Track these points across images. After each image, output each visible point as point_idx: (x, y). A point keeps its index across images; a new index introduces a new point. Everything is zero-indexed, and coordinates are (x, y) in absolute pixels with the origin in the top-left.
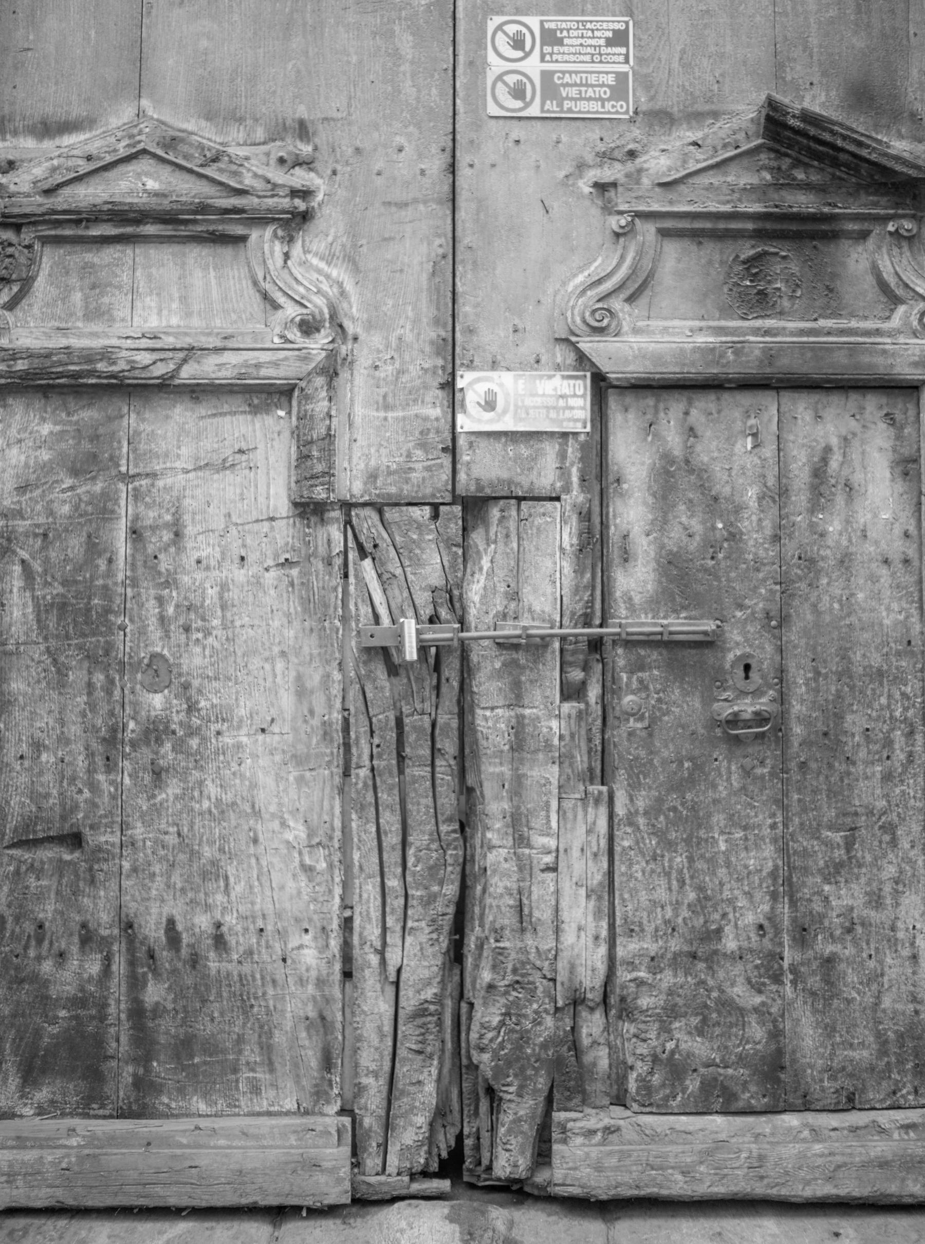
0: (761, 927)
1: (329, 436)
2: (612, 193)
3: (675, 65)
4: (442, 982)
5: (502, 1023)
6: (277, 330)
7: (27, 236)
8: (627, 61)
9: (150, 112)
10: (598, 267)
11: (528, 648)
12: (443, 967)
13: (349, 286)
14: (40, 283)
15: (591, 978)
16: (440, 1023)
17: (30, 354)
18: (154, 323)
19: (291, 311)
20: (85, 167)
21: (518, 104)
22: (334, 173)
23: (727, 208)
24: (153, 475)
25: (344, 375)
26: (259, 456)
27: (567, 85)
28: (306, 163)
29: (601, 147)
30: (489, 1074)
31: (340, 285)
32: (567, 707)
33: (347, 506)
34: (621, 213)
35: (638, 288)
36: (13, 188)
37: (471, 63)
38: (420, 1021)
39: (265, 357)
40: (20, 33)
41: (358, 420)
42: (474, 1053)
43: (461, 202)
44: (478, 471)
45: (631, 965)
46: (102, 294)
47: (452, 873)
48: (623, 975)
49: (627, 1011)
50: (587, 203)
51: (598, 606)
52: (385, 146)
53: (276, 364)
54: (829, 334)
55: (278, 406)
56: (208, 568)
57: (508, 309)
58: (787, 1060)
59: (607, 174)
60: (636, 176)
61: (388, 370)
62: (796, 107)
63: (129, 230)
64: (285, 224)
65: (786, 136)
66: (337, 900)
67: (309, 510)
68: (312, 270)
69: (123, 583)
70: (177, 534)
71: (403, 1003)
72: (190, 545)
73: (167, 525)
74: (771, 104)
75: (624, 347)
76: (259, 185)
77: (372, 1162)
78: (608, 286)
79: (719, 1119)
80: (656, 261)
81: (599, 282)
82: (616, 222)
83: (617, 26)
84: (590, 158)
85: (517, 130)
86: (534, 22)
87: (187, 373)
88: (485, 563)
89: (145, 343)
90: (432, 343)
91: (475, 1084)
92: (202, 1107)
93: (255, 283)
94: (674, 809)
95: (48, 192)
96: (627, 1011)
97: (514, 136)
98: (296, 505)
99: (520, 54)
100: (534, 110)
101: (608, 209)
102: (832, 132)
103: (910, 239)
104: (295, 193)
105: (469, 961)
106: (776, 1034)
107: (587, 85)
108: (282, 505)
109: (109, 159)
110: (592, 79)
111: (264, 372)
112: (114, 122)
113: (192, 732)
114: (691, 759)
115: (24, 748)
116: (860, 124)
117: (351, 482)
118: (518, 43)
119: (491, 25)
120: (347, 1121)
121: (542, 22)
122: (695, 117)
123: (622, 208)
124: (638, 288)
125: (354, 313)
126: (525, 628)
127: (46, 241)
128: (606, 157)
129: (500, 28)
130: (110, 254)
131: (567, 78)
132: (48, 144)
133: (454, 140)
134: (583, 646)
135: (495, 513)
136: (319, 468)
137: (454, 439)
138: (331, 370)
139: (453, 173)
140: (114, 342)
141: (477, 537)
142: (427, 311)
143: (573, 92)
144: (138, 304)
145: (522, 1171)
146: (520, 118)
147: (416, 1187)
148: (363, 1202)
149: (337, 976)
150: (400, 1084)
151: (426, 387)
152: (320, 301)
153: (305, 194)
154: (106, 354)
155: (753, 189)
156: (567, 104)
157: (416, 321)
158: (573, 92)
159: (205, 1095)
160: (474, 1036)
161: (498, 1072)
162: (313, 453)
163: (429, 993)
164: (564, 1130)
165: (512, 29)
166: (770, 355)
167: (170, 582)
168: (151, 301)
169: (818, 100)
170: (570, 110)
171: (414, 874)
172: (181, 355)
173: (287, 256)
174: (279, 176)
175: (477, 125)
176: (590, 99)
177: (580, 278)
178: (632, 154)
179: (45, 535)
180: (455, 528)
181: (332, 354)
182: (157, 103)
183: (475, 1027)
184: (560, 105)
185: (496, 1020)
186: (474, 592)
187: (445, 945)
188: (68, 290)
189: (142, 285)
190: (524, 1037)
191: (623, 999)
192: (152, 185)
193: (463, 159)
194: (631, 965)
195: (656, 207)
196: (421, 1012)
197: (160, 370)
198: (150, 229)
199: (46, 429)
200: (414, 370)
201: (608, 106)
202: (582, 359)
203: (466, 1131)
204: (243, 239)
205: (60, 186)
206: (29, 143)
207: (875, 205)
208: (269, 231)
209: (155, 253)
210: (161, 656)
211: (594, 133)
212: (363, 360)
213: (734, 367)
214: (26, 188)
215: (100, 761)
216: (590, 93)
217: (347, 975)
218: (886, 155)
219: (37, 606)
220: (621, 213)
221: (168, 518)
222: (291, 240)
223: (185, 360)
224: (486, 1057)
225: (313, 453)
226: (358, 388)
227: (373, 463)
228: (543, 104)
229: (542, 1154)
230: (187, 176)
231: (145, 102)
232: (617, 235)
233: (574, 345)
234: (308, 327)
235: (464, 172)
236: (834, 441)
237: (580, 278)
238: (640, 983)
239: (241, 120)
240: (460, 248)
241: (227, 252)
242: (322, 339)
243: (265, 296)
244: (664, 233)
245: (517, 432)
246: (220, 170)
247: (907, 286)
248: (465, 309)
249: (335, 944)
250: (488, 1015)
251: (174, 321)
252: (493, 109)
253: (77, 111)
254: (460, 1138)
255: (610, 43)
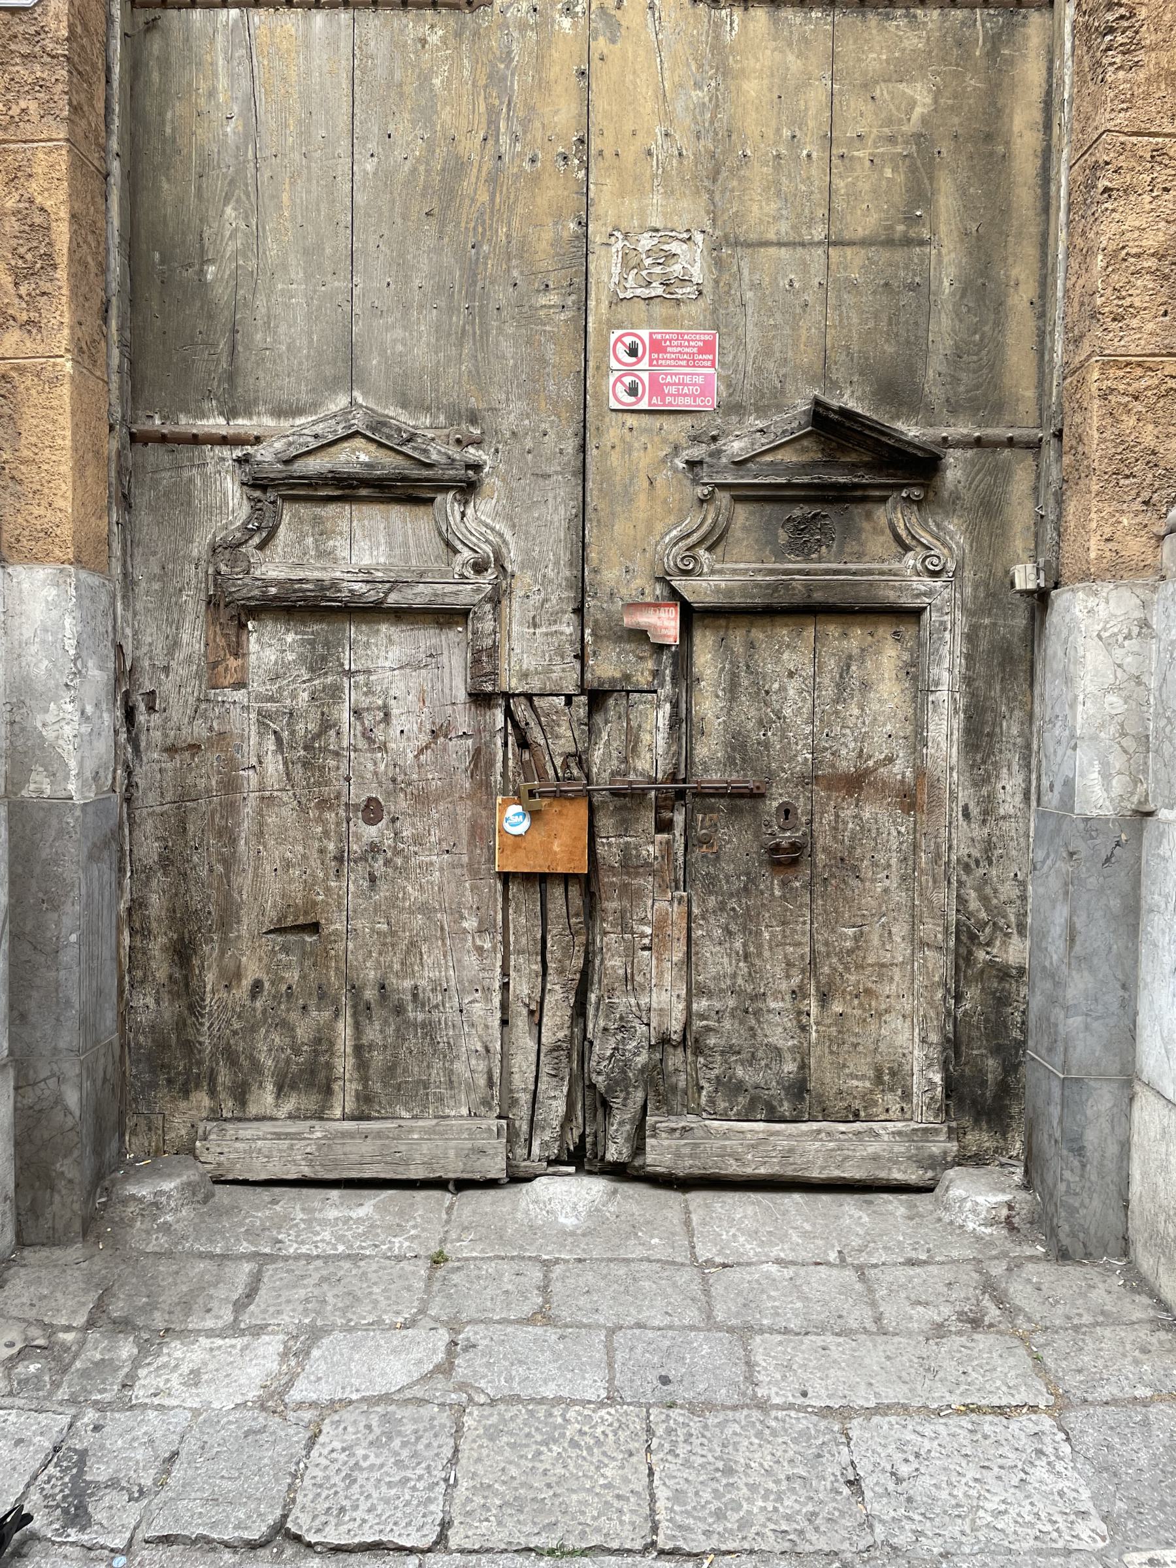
0: (794, 992)
1: (495, 647)
2: (697, 469)
3: (749, 368)
4: (571, 1027)
5: (612, 1055)
6: (457, 569)
7: (271, 495)
8: (713, 366)
9: (360, 400)
10: (690, 523)
11: (632, 796)
12: (572, 1017)
13: (508, 536)
14: (282, 529)
15: (675, 1026)
16: (569, 1056)
17: (278, 583)
18: (366, 561)
19: (466, 554)
20: (314, 444)
21: (633, 399)
22: (497, 451)
23: (782, 480)
24: (368, 672)
25: (505, 602)
26: (444, 659)
27: (669, 384)
28: (477, 443)
29: (692, 433)
30: (603, 1090)
31: (501, 536)
32: (659, 837)
33: (507, 696)
34: (705, 484)
35: (715, 540)
36: (259, 458)
37: (598, 368)
38: (556, 1054)
39: (449, 588)
40: (259, 336)
41: (514, 635)
42: (594, 1076)
43: (590, 476)
44: (599, 672)
45: (703, 1017)
46: (329, 539)
47: (579, 951)
48: (698, 1024)
49: (698, 1050)
50: (680, 476)
51: (683, 766)
52: (534, 431)
53: (456, 593)
54: (854, 574)
55: (458, 624)
56: (408, 739)
57: (622, 555)
58: (811, 1085)
59: (697, 452)
60: (717, 453)
61: (536, 599)
62: (835, 403)
63: (347, 492)
64: (461, 490)
65: (829, 425)
66: (499, 970)
67: (480, 699)
68: (480, 521)
69: (348, 749)
70: (386, 714)
71: (544, 1040)
72: (394, 722)
73: (379, 708)
74: (817, 402)
75: (704, 584)
76: (443, 460)
77: (521, 1152)
78: (695, 537)
79: (761, 1126)
80: (729, 521)
81: (688, 535)
82: (701, 491)
83: (707, 338)
84: (684, 442)
85: (631, 420)
86: (644, 334)
87: (393, 598)
88: (605, 736)
89: (361, 576)
90: (566, 579)
91: (594, 1100)
92: (404, 1114)
93: (440, 533)
94: (733, 909)
95: (288, 462)
96: (698, 1050)
97: (628, 425)
98: (470, 695)
99: (634, 360)
100: (644, 405)
101: (696, 481)
102: (863, 424)
103: (919, 503)
104: (468, 467)
105: (591, 1011)
106: (803, 1066)
107: (684, 384)
108: (461, 695)
109: (331, 437)
110: (687, 379)
111: (447, 600)
112: (333, 408)
113: (397, 852)
114: (748, 874)
115: (277, 865)
116: (881, 417)
117: (510, 682)
118: (633, 352)
119: (613, 337)
120: (504, 1122)
121: (651, 334)
122: (761, 410)
123: (706, 480)
124: (715, 540)
125: (513, 557)
126: (631, 782)
127: (285, 498)
128: (696, 439)
129: (619, 339)
130: (331, 510)
131: (669, 379)
132: (285, 423)
133: (584, 427)
134: (672, 795)
135: (611, 702)
136: (488, 669)
137: (583, 649)
138: (496, 598)
139: (584, 452)
140: (338, 574)
141: (599, 719)
142: (565, 557)
143: (673, 390)
144: (355, 547)
145: (624, 1158)
146: (633, 411)
147: (551, 1170)
148: (517, 1178)
149: (497, 1023)
150: (540, 1096)
151: (564, 612)
152: (488, 549)
153: (477, 467)
154: (334, 585)
155: (804, 466)
156: (668, 399)
157: (557, 563)
158: (673, 390)
159: (405, 1105)
160: (593, 1064)
161: (609, 1089)
162: (483, 660)
163: (561, 1035)
164: (654, 1128)
165: (628, 340)
166: (809, 588)
167: (383, 748)
168: (365, 544)
169: (850, 400)
170: (670, 404)
171: (552, 952)
172: (388, 585)
173: (463, 515)
174: (454, 451)
175: (600, 416)
176: (686, 395)
177: (674, 533)
178: (714, 439)
179: (291, 714)
180: (583, 712)
181: (496, 587)
182: (365, 394)
183: (595, 1058)
184: (663, 400)
185: (608, 1053)
186: (597, 755)
187: (572, 1001)
188: (303, 536)
189: (358, 534)
190: (627, 1064)
191: (697, 1040)
192: (364, 458)
193: (591, 443)
194: (703, 1017)
195: (730, 480)
196: (556, 1048)
197: (372, 596)
198: (364, 492)
199: (290, 638)
200: (554, 599)
201: (698, 401)
202: (675, 594)
203: (588, 1131)
204: (431, 501)
205: (296, 457)
206: (269, 421)
207: (894, 476)
208: (450, 495)
209: (368, 510)
210: (376, 799)
211: (686, 422)
212: (519, 592)
213: (781, 599)
214: (269, 457)
215: (332, 873)
216: (686, 391)
217: (504, 1022)
218: (901, 440)
219: (285, 763)
220: (705, 484)
221: (380, 702)
222: (466, 503)
223: (390, 590)
224: (601, 1078)
225: (483, 660)
226: (516, 610)
227: (525, 667)
228: (650, 399)
229: (639, 1149)
230: (389, 453)
231: (356, 393)
232: (702, 501)
233: (668, 583)
234: (479, 568)
235: (592, 452)
236: (855, 651)
237: (674, 533)
238: (708, 1029)
239: (428, 409)
240: (589, 509)
241: (420, 511)
242: (490, 575)
243: (448, 544)
244: (737, 499)
245: (535, 874)
246: (414, 448)
247: (914, 537)
248: (593, 555)
249: (497, 999)
250: (602, 1048)
251: (382, 560)
252: (614, 405)
253: (305, 398)
254: (582, 1137)
255: (701, 351)
